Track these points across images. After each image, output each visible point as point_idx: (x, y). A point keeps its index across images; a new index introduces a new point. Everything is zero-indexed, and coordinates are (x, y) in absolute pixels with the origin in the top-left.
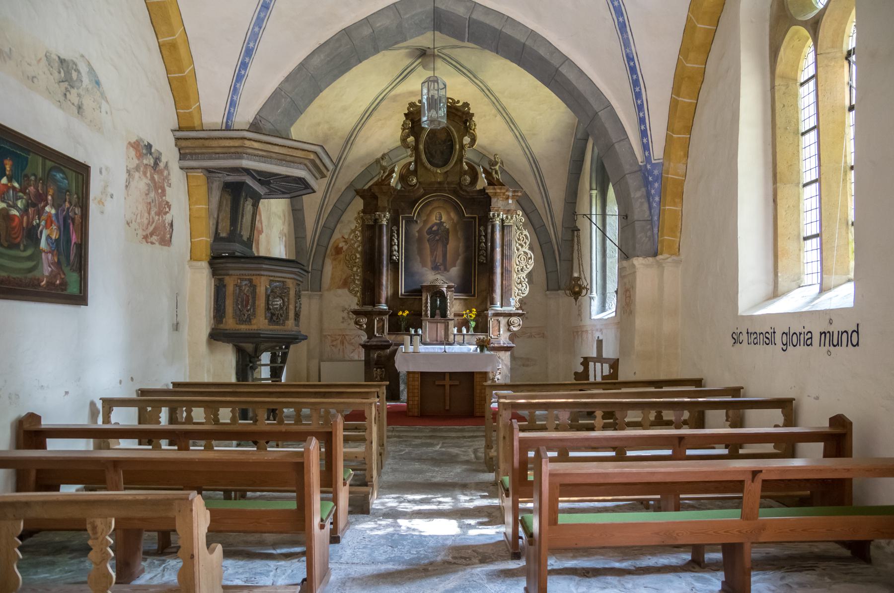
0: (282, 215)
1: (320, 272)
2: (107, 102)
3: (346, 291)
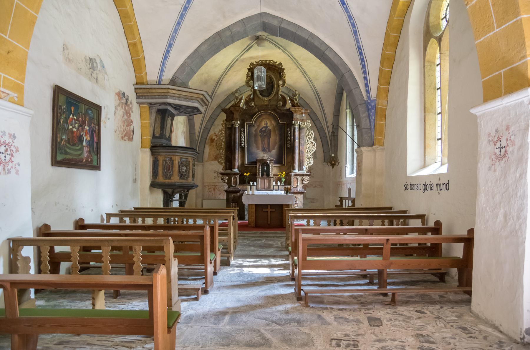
0: (183, 122)
1: (202, 152)
2: (107, 75)
3: (216, 162)
